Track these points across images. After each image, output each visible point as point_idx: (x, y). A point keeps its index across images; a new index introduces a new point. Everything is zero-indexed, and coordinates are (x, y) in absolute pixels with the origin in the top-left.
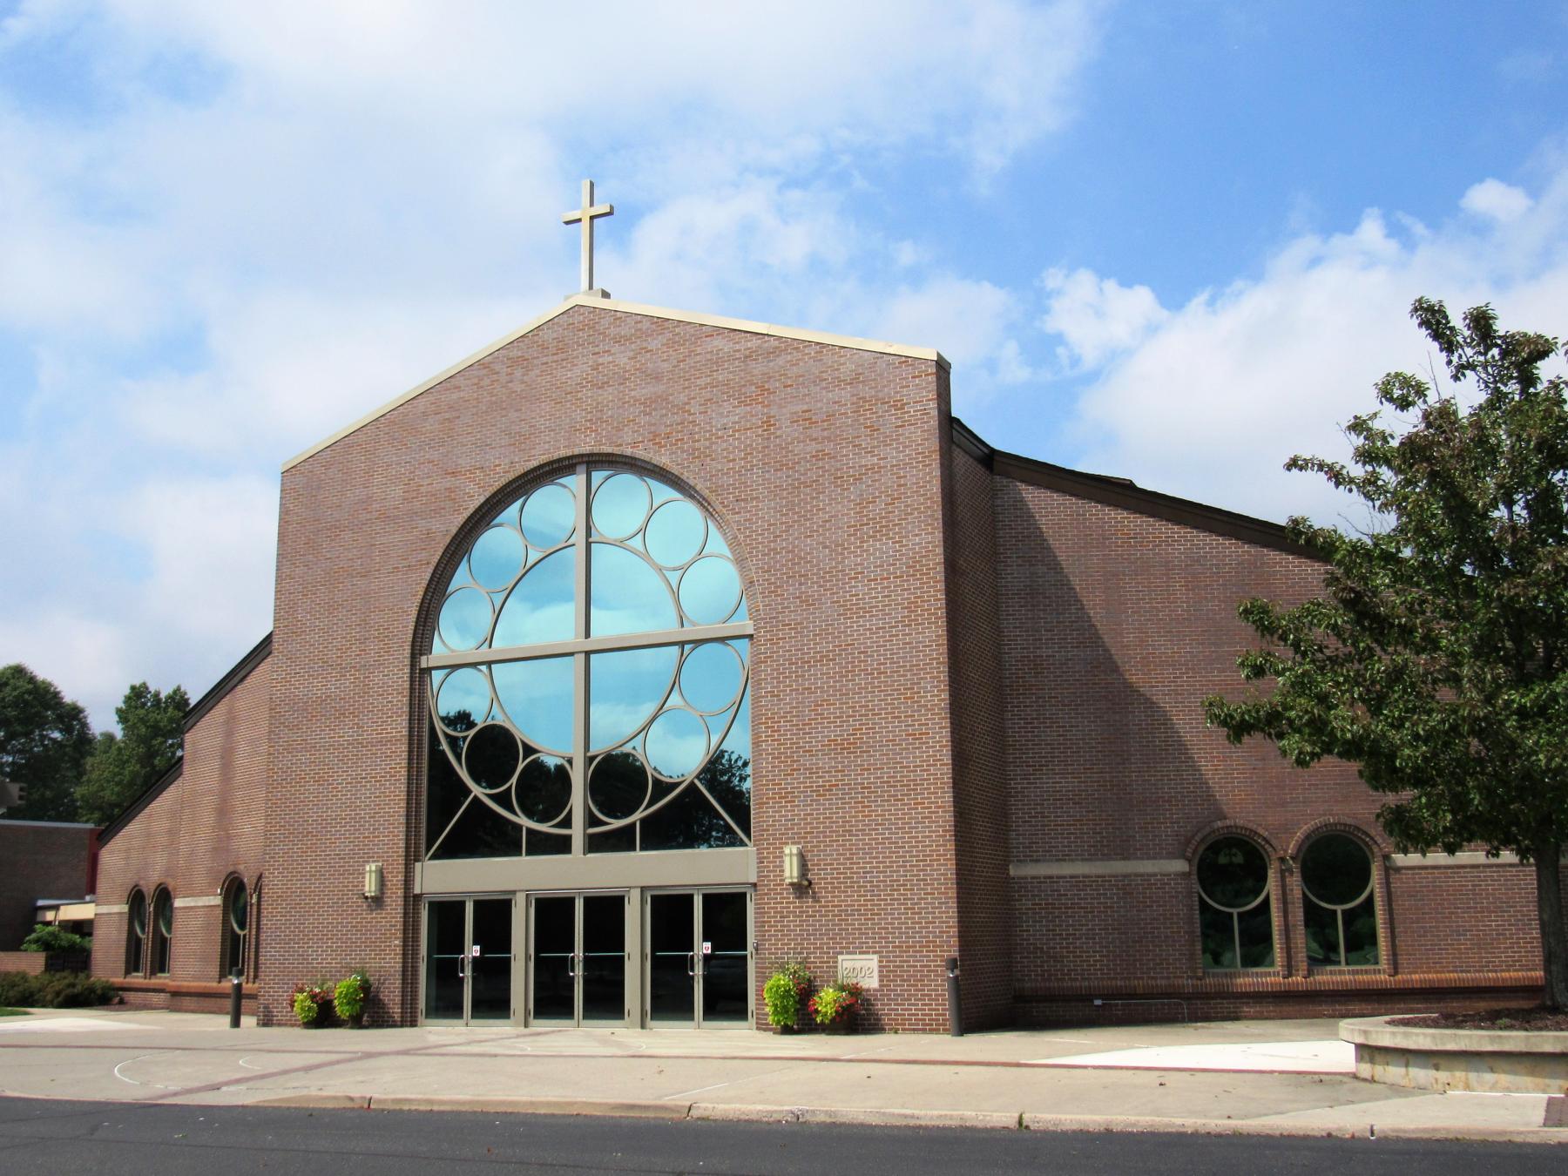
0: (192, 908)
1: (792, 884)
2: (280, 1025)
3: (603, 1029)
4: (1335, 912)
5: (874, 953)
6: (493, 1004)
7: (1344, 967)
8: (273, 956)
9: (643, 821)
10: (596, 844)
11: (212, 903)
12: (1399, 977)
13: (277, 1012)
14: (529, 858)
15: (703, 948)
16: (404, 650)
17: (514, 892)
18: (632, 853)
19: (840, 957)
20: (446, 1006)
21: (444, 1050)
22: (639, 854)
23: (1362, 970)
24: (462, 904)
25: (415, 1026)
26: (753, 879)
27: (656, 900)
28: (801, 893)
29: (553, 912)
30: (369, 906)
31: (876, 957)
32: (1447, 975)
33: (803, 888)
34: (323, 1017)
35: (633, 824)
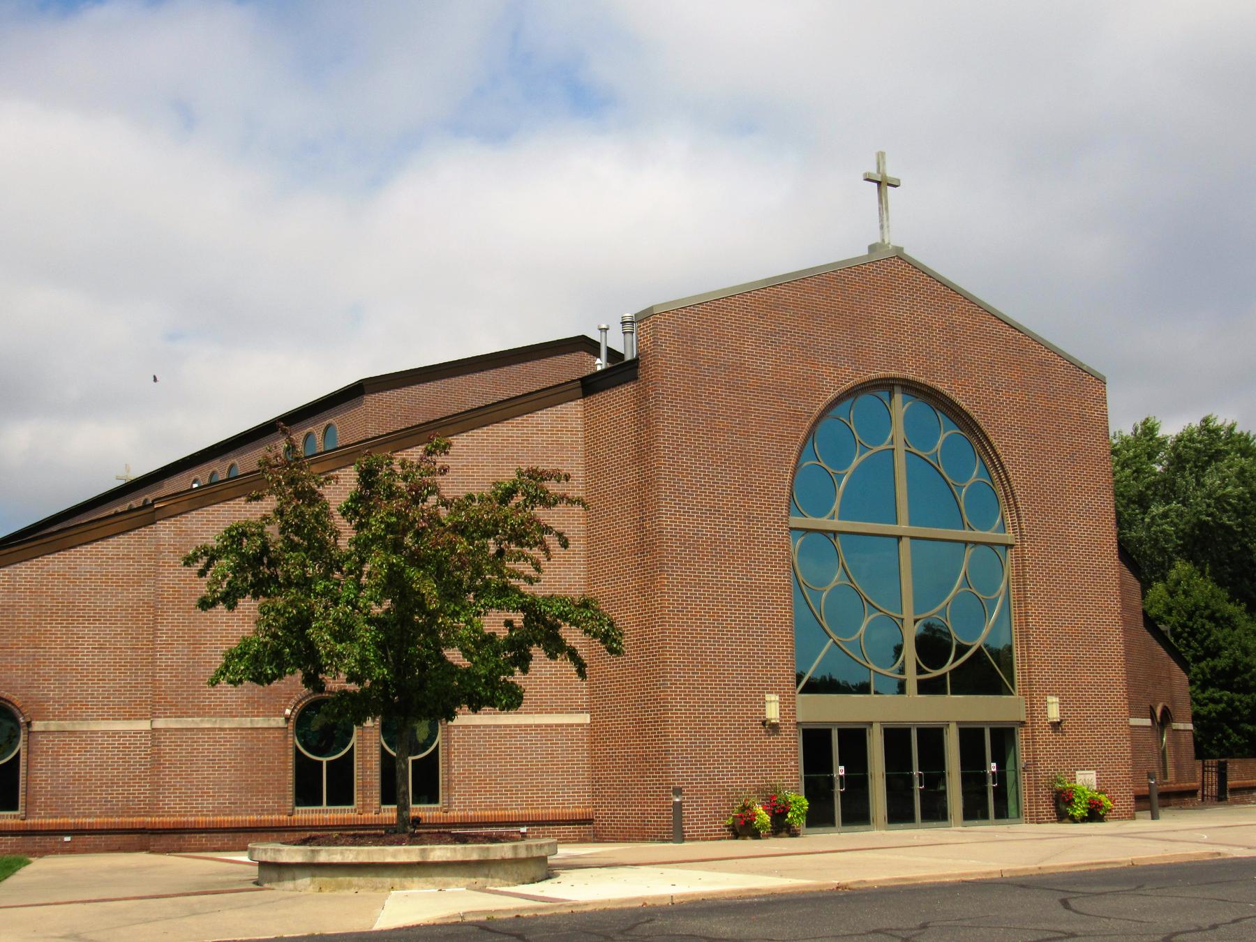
0: (203, 729)
1: (1051, 723)
2: (693, 840)
3: (859, 836)
4: (322, 762)
5: (1094, 769)
6: (857, 815)
7: (325, 807)
8: (681, 776)
9: (951, 672)
10: (927, 687)
11: (1144, 724)
12: (29, 821)
13: (688, 828)
14: (953, 696)
15: (841, 771)
16: (782, 509)
17: (871, 724)
18: (867, 696)
19: (1077, 772)
20: (819, 817)
21: (1153, 835)
22: (950, 697)
23: (430, 808)
24: (828, 732)
25: (1158, 819)
26: (1023, 718)
27: (885, 730)
28: (1055, 729)
29: (896, 738)
30: (767, 732)
31: (1094, 772)
32: (201, 818)
33: (1056, 726)
34: (744, 829)
35: (945, 675)
